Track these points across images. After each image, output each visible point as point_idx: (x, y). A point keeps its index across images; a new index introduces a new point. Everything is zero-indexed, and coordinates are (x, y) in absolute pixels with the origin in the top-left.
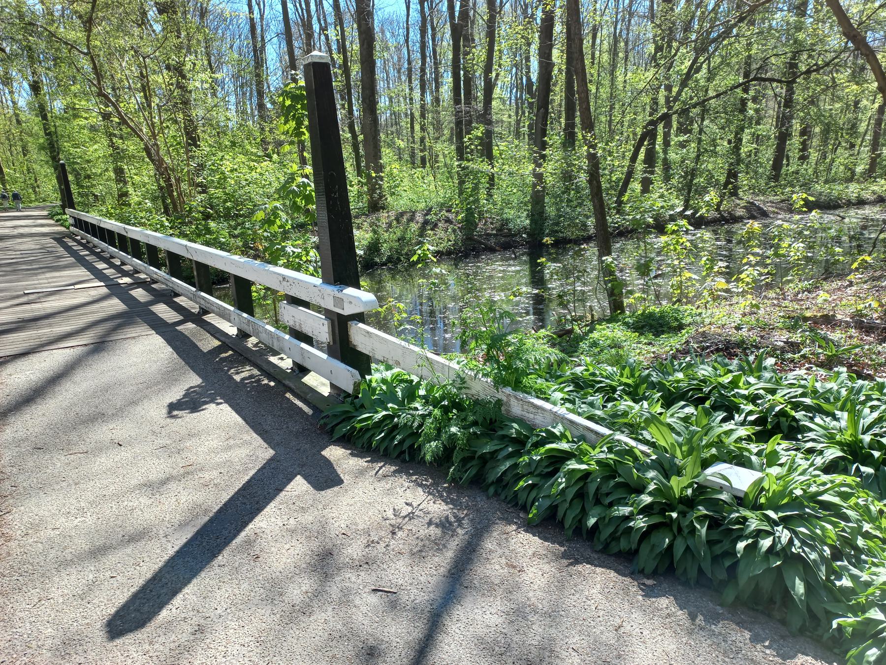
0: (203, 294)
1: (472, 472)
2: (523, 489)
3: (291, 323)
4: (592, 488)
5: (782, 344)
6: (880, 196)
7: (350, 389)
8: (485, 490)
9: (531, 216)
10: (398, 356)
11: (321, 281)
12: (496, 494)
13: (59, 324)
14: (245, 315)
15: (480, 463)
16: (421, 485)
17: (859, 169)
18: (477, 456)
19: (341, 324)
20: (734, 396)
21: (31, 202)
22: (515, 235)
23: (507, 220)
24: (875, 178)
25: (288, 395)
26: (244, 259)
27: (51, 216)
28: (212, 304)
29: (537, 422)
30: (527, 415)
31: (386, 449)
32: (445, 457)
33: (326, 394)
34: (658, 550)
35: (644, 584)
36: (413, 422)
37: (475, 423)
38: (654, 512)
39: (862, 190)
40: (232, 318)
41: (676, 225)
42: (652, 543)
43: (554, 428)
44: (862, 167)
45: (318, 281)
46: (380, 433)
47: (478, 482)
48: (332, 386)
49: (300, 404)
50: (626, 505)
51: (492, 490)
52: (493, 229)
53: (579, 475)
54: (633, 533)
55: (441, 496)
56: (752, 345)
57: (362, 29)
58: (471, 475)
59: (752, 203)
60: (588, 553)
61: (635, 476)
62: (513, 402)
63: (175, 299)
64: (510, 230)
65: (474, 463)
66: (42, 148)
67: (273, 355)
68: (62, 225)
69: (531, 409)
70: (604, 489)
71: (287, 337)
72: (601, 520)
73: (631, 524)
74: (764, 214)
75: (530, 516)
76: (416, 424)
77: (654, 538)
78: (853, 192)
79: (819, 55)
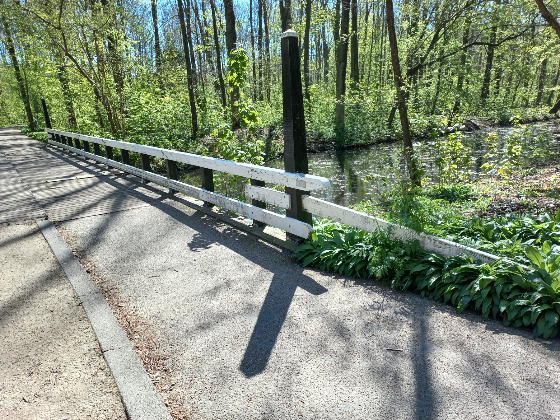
0: (173, 180)
1: (408, 283)
2: (449, 292)
3: (255, 197)
4: (499, 290)
5: (553, 205)
6: (545, 117)
7: (306, 237)
8: (418, 293)
9: (336, 130)
10: (331, 217)
11: (284, 171)
12: (426, 296)
13: (81, 199)
14: (212, 193)
15: (411, 277)
16: (376, 292)
17: (531, 100)
18: (410, 273)
19: (296, 195)
20: (553, 235)
21: (6, 124)
22: (327, 142)
23: (321, 133)
24: (541, 105)
25: (260, 240)
26: (208, 158)
27: (24, 133)
28: (179, 186)
29: (445, 253)
30: (437, 249)
31: (343, 272)
32: (389, 275)
33: (285, 240)
34: (551, 325)
35: (546, 344)
36: (362, 254)
37: (405, 254)
38: (543, 302)
39: (535, 112)
40: (201, 195)
41: (455, 135)
42: (547, 319)
43: (461, 256)
44: (533, 98)
45: (283, 171)
46: (338, 262)
47: (413, 290)
48: (288, 234)
49: (270, 245)
50: (522, 299)
51: (423, 294)
52: (312, 139)
53: (488, 283)
54: (532, 315)
55: (393, 298)
56: (534, 206)
57: (228, 12)
58: (408, 285)
59: (469, 121)
60: (501, 327)
61: (524, 281)
62: (427, 241)
63: (148, 184)
64: (323, 139)
65: (408, 278)
66: (15, 89)
67: (235, 217)
68: (34, 138)
69: (441, 245)
70: (506, 290)
71: (250, 205)
72: (508, 307)
73: (530, 309)
74: (478, 128)
75: (458, 307)
76: (364, 256)
77: (548, 317)
78: (530, 114)
79: (86, 7)
